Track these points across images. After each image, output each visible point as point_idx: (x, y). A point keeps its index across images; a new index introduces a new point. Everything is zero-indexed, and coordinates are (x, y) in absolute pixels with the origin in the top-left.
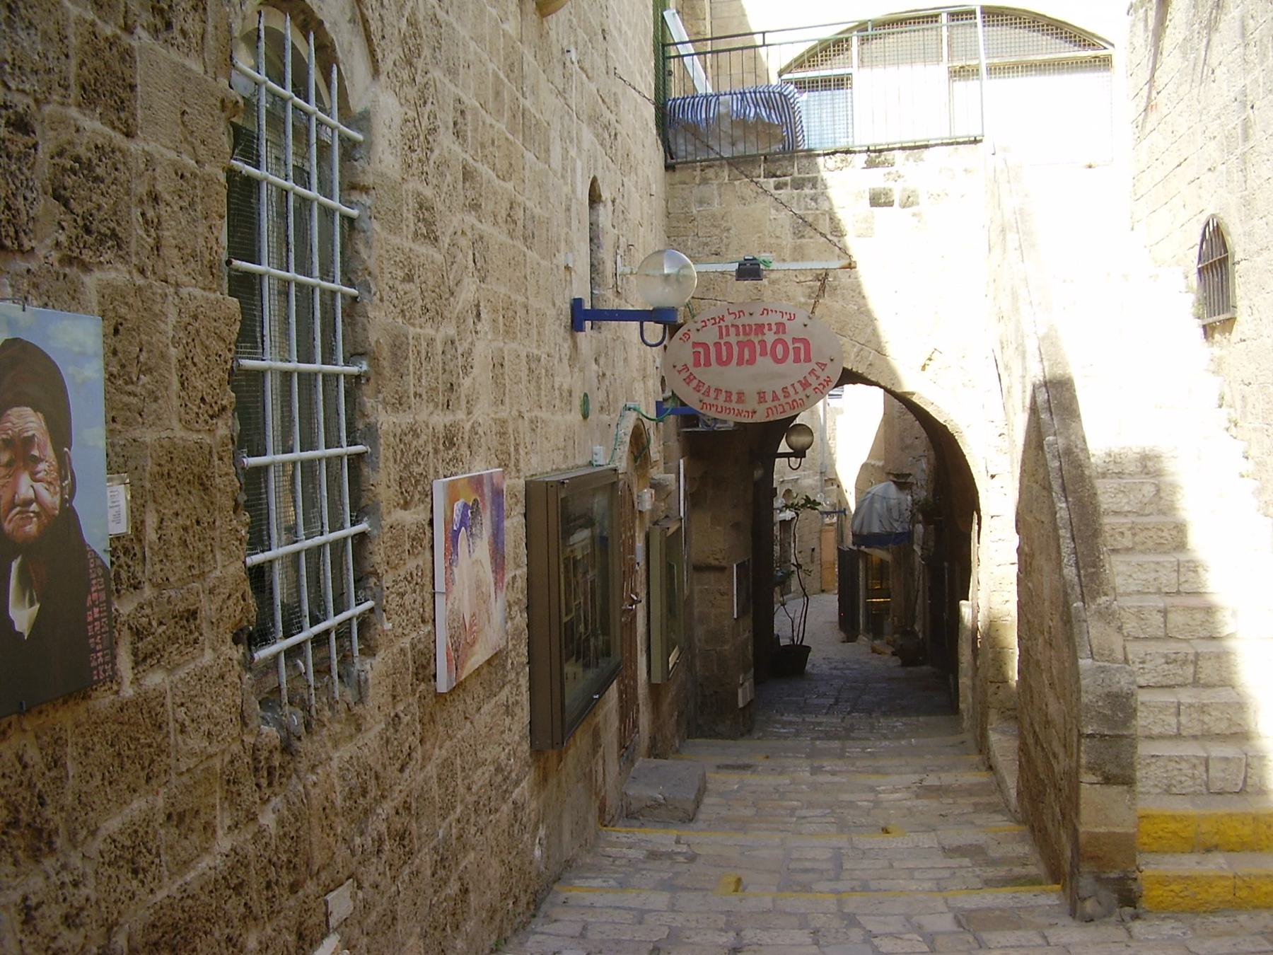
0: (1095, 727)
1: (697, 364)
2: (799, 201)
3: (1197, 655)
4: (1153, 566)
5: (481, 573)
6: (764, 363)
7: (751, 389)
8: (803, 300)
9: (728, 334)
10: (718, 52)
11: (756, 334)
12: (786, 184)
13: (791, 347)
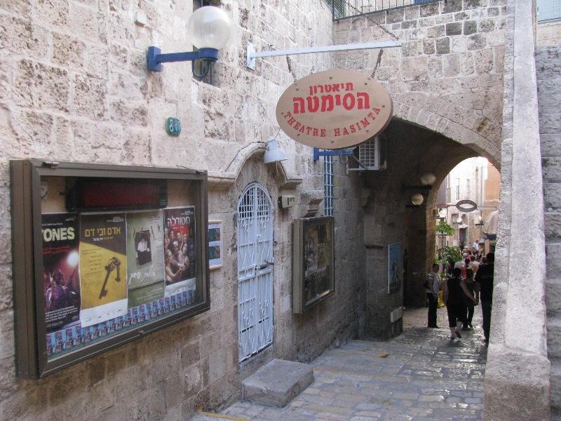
1: (296, 111)
2: (406, 35)
6: (339, 110)
7: (330, 127)
8: (408, 91)
9: (316, 92)
11: (334, 91)
12: (398, 26)
13: (356, 98)
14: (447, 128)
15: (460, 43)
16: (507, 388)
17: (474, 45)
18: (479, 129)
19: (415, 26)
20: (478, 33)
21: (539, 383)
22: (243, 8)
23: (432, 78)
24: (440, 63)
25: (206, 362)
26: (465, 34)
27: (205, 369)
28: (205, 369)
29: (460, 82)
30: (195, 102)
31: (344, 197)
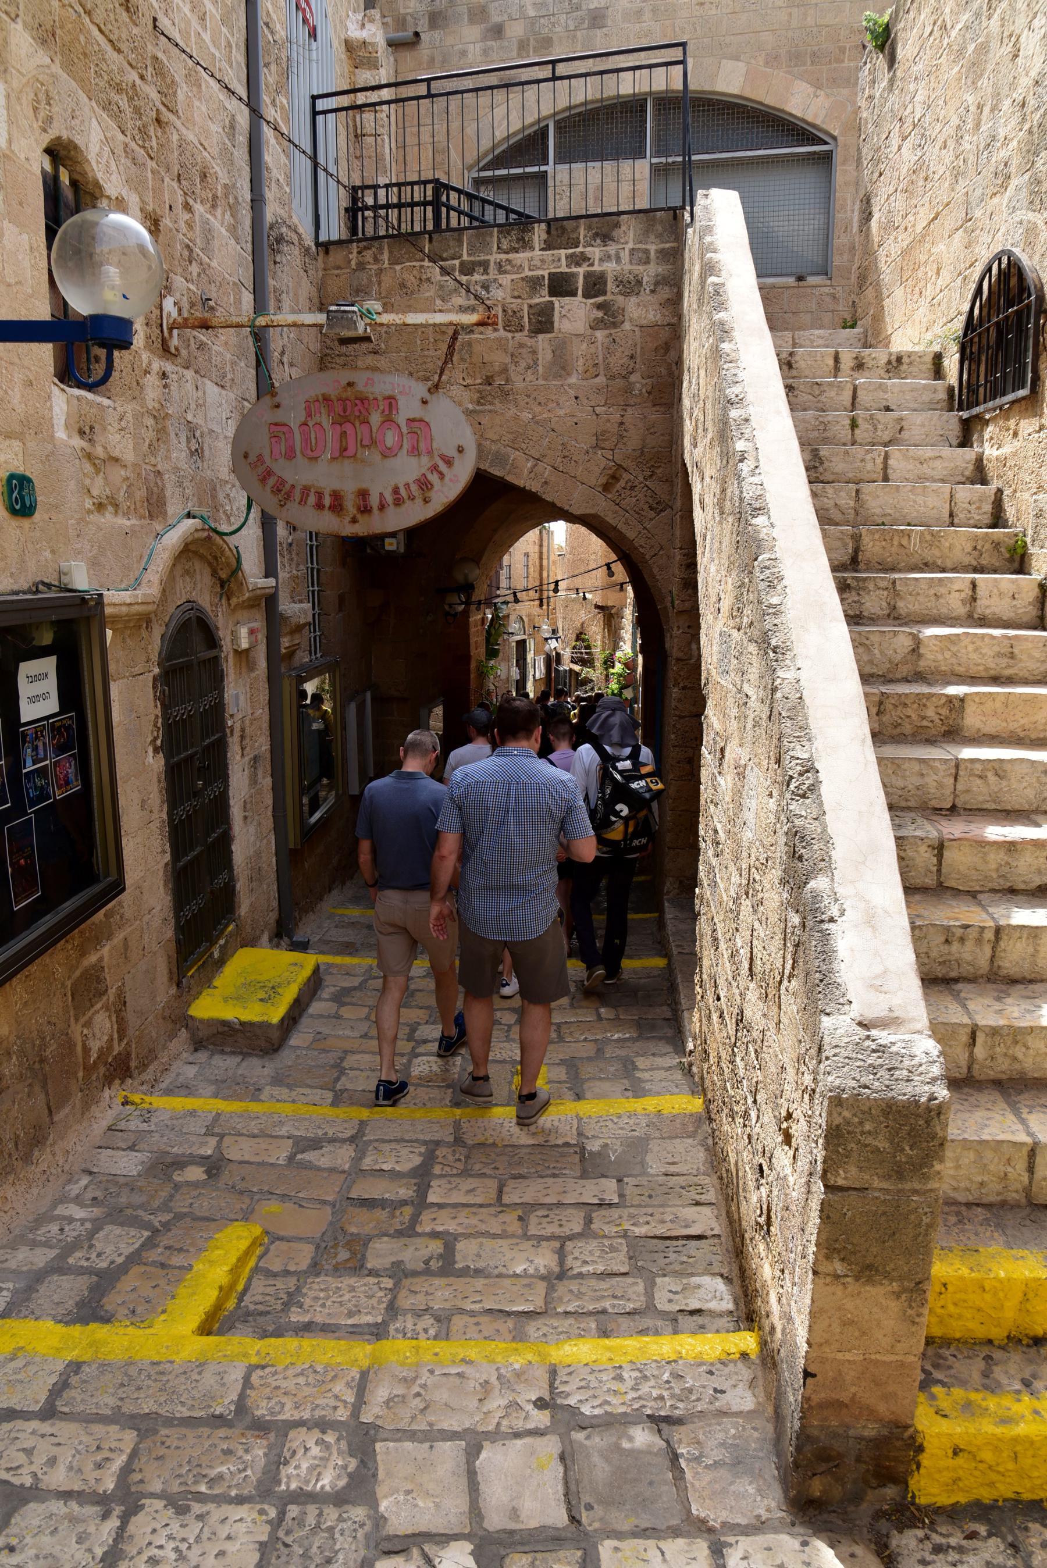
0: (853, 1170)
3: (998, 931)
4: (916, 767)
5: (159, 134)
10: (403, 100)
14: (546, 483)
15: (574, 314)
16: (873, 1111)
17: (602, 320)
18: (606, 488)
19: (486, 272)
20: (609, 297)
21: (932, 1098)
22: (150, 208)
23: (519, 384)
24: (534, 352)
25: (120, 994)
26: (586, 296)
27: (119, 1010)
28: (119, 1010)
29: (572, 393)
30: (61, 434)
31: (340, 610)
